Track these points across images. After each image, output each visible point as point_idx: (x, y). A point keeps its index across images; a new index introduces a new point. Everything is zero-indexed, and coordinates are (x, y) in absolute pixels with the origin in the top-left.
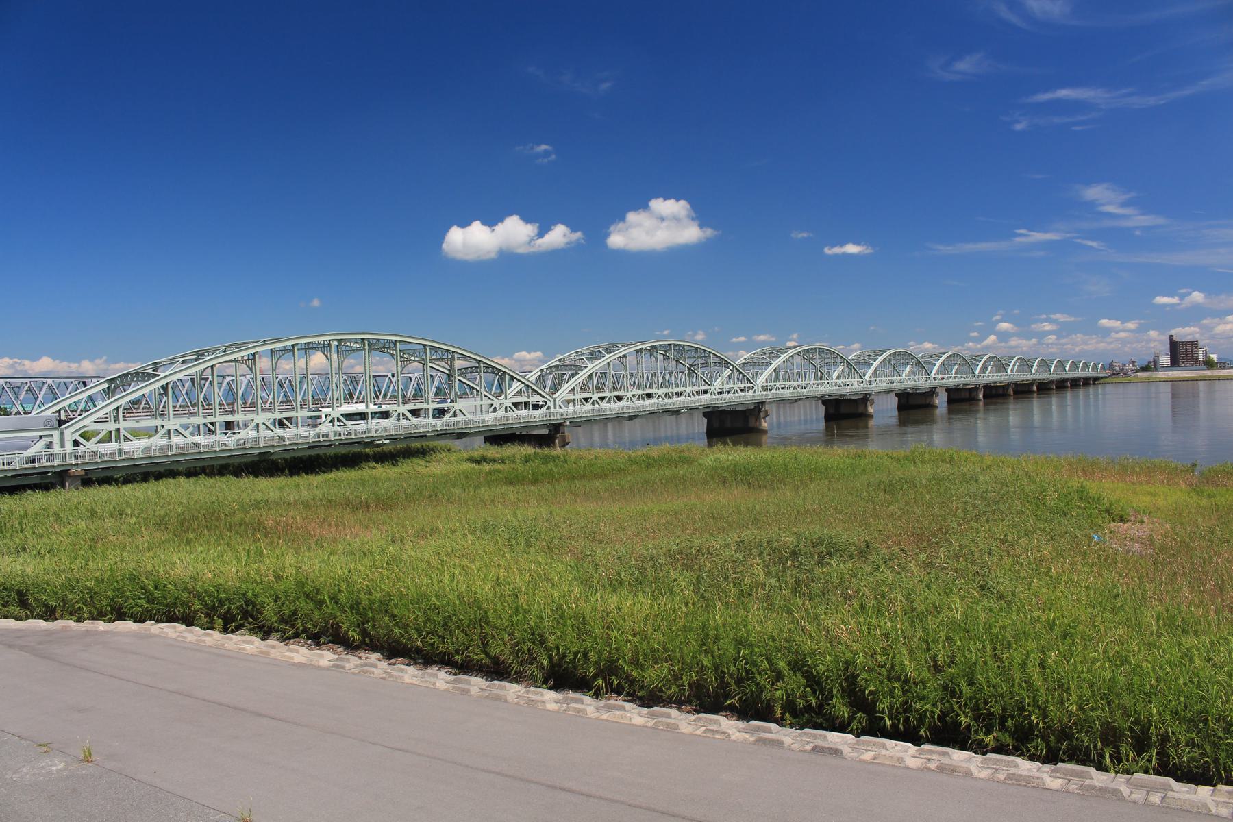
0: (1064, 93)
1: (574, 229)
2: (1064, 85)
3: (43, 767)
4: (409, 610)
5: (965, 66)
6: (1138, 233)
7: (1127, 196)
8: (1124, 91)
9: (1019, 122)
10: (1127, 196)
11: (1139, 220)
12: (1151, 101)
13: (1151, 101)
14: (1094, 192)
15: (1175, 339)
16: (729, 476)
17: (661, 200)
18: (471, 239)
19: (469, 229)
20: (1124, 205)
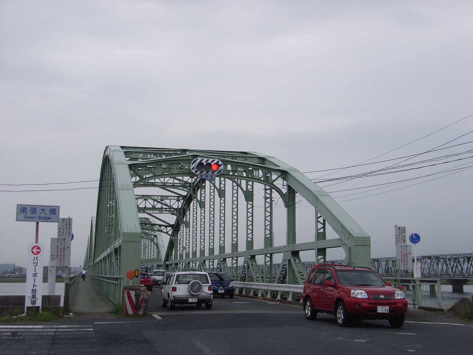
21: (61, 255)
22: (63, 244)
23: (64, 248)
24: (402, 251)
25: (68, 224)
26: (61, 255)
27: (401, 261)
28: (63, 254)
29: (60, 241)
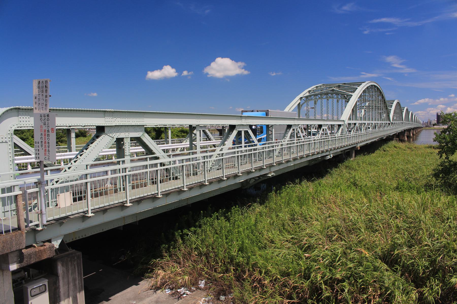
0: (384, 20)
1: (245, 68)
2: (384, 17)
3: (259, 290)
4: (363, 206)
5: (347, 8)
6: (406, 75)
7: (402, 61)
8: (406, 20)
9: (366, 30)
10: (402, 61)
11: (407, 70)
12: (416, 24)
13: (416, 24)
14: (390, 59)
15: (439, 114)
16: (253, 192)
17: (220, 58)
18: (155, 75)
19: (163, 70)
20: (401, 64)
21: (45, 142)
22: (47, 124)
23: (48, 131)
24: (41, 127)
25: (44, 89)
26: (45, 142)
27: (40, 144)
28: (47, 141)
29: (43, 118)
